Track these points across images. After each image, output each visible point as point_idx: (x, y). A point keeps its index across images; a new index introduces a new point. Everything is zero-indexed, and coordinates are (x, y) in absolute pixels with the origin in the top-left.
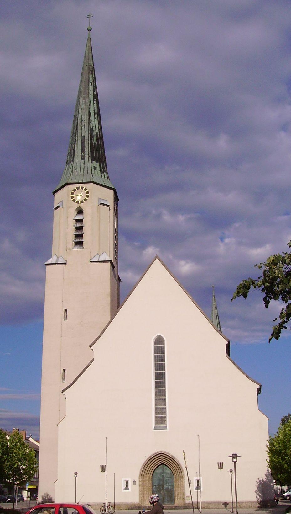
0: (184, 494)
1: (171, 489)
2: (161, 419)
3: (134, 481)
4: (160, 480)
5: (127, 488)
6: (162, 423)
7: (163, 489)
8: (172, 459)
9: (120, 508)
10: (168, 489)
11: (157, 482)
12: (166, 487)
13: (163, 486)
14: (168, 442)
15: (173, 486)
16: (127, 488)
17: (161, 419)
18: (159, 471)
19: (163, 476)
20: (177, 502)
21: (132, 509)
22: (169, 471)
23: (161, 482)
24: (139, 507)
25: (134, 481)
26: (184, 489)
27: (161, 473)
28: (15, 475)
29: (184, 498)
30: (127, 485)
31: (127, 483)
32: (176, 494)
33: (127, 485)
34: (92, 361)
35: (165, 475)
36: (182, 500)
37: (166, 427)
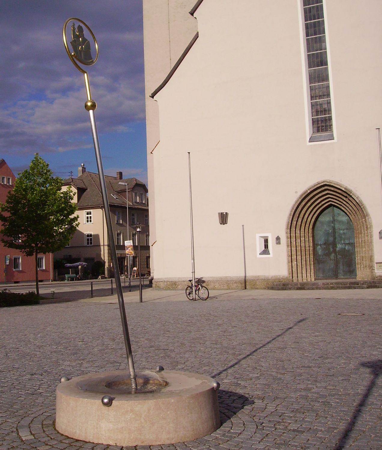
0: (371, 258)
1: (348, 251)
2: (322, 123)
3: (278, 239)
4: (328, 234)
5: (266, 251)
6: (326, 130)
7: (334, 251)
8: (345, 195)
9: (254, 287)
10: (343, 250)
11: (323, 239)
12: (339, 246)
13: (334, 244)
14: (342, 163)
15: (352, 245)
16: (266, 251)
17: (322, 123)
18: (326, 218)
19: (334, 228)
20: (361, 274)
21: (272, 288)
22: (345, 219)
23: (331, 239)
24: (284, 285)
25: (278, 239)
26: (372, 250)
27: (329, 222)
28: (34, 197)
29: (371, 267)
30: (266, 246)
31: (266, 241)
32: (358, 259)
33: (266, 246)
34: (197, 37)
35: (337, 226)
36: (368, 271)
37: (332, 135)
